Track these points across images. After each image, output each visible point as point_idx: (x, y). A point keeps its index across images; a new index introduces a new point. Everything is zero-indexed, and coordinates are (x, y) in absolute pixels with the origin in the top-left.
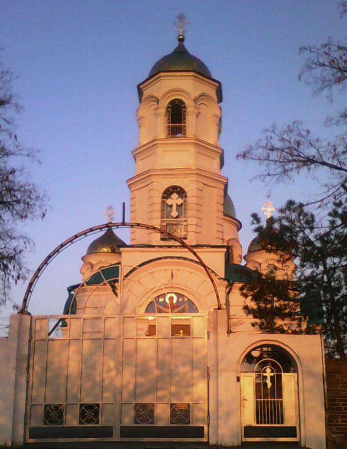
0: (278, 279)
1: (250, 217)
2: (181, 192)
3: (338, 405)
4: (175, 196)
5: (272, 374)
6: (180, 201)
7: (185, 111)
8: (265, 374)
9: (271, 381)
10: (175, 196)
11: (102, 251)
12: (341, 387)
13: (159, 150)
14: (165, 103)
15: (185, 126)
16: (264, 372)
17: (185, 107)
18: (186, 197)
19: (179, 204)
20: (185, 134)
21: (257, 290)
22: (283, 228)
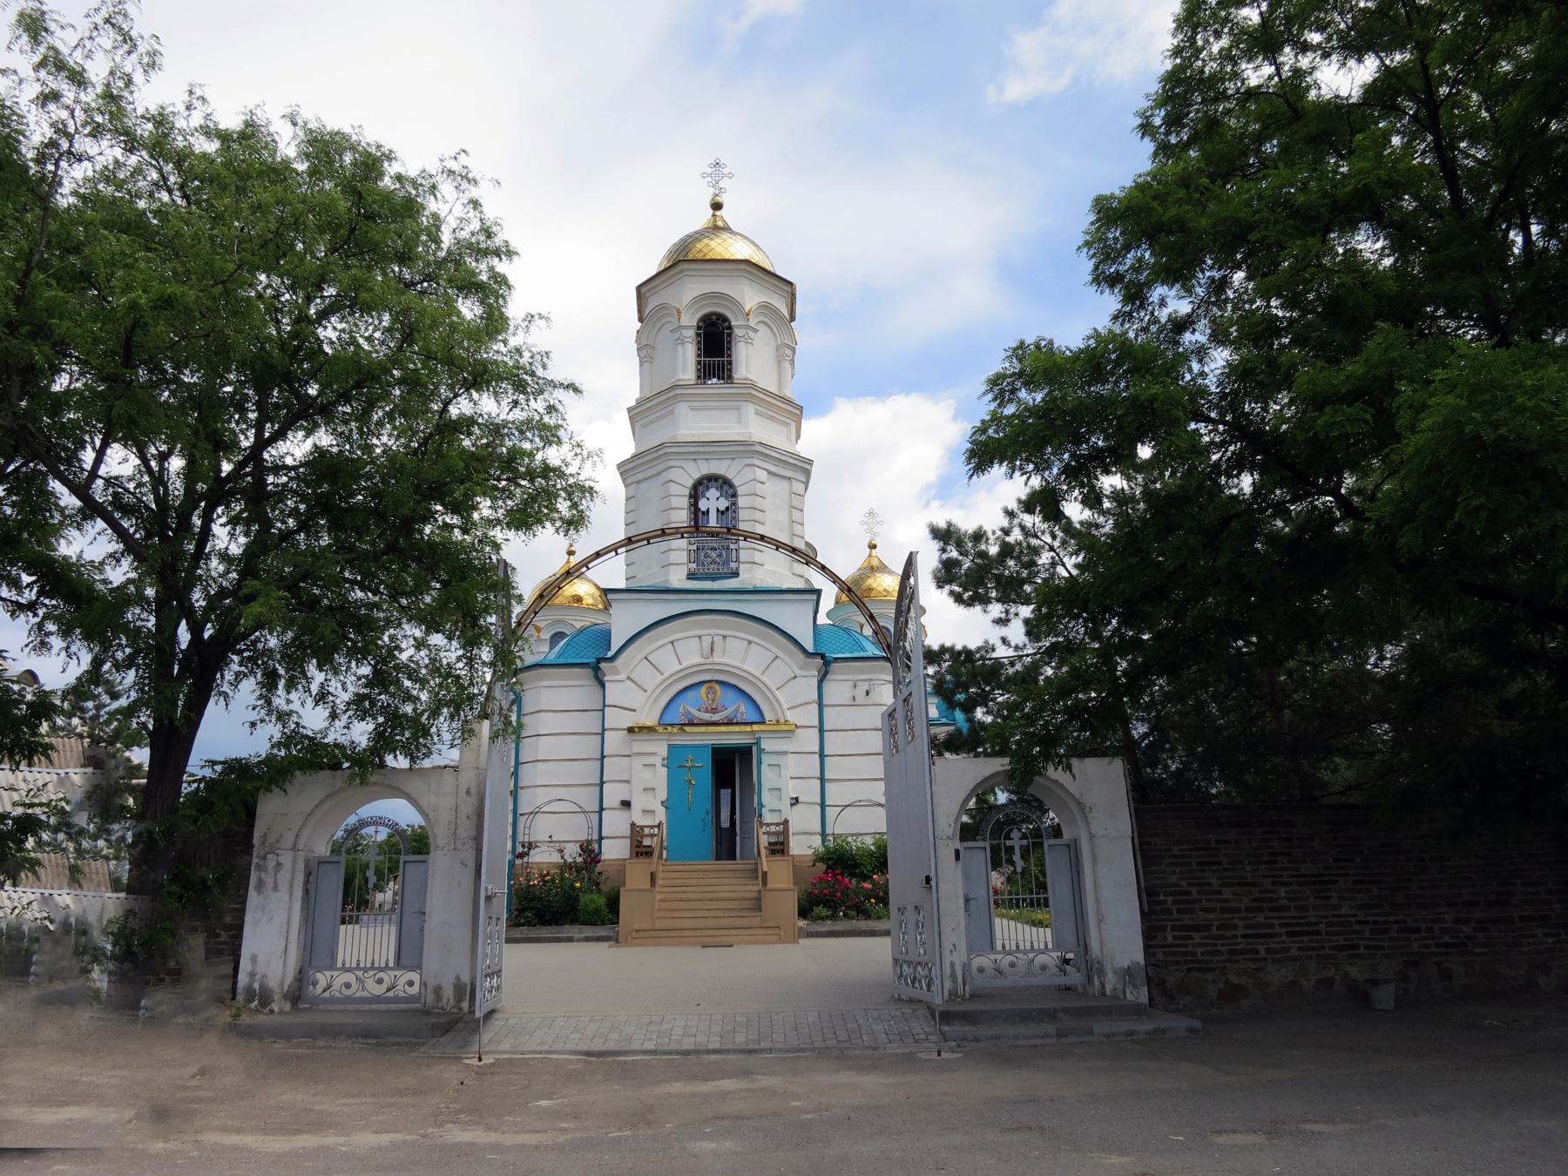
0: (1327, 94)
1: (164, 67)
2: (724, 484)
3: (1165, 902)
4: (713, 493)
5: (1025, 842)
6: (723, 504)
7: (730, 335)
8: (1008, 843)
9: (1023, 857)
10: (713, 493)
11: (88, 466)
12: (1170, 865)
13: (682, 409)
14: (690, 320)
15: (730, 363)
16: (1008, 837)
17: (730, 327)
18: (734, 495)
19: (722, 508)
20: (730, 377)
21: (410, 1137)
22: (1007, 550)
